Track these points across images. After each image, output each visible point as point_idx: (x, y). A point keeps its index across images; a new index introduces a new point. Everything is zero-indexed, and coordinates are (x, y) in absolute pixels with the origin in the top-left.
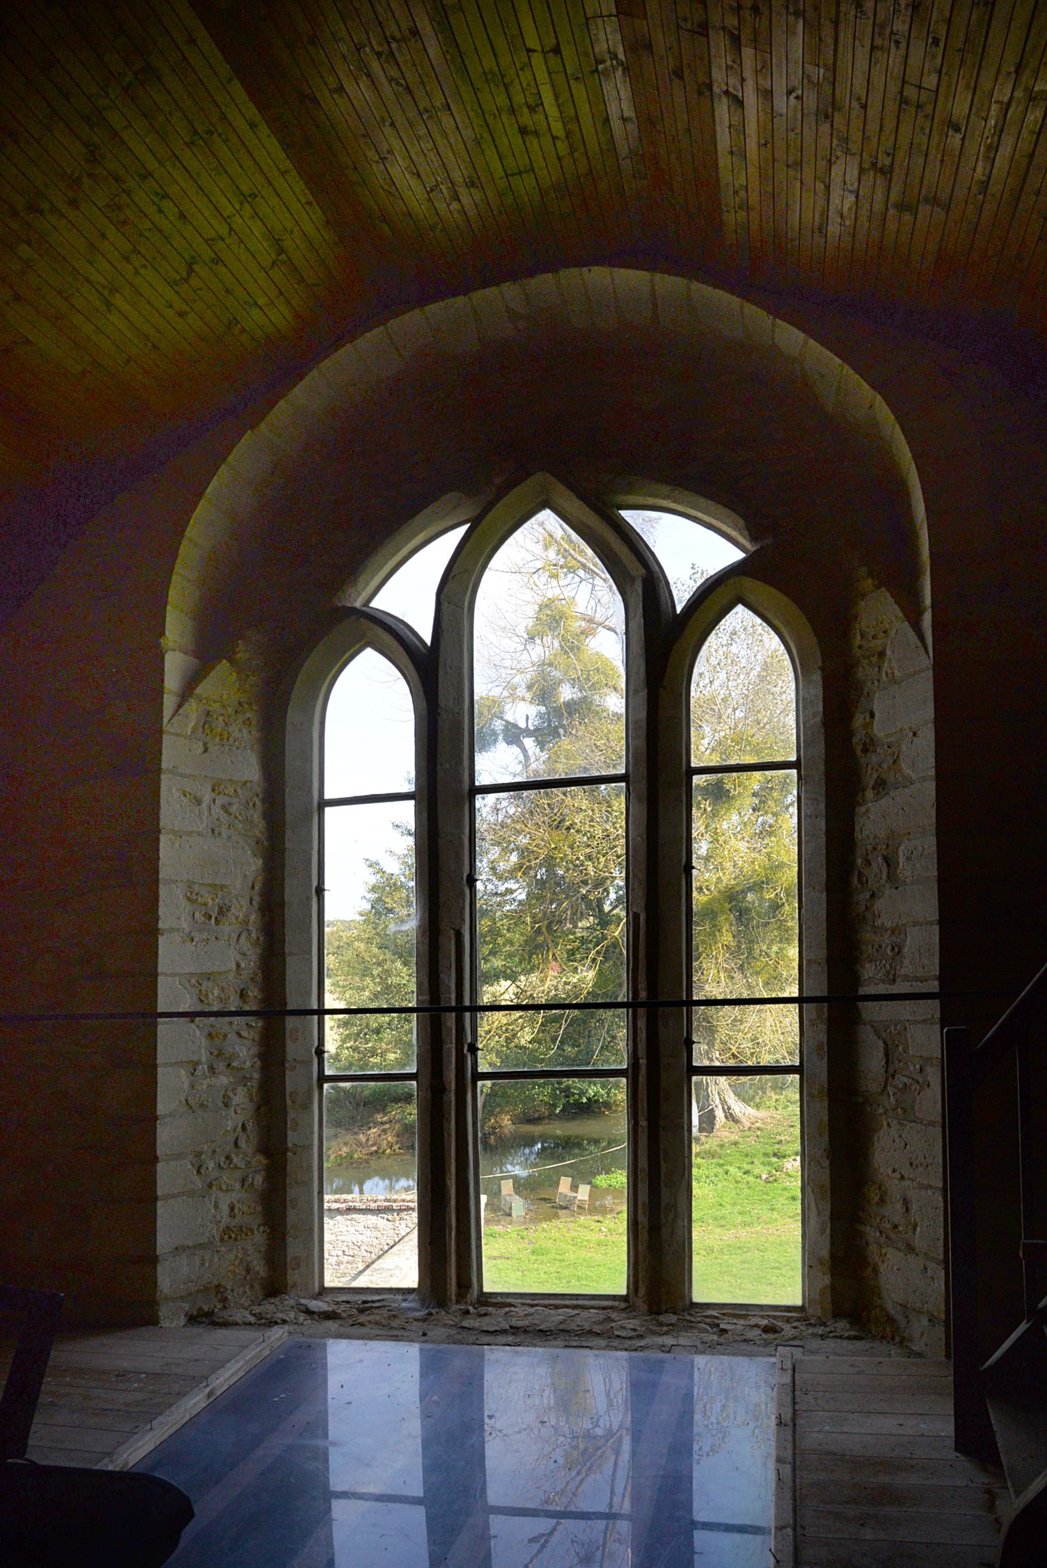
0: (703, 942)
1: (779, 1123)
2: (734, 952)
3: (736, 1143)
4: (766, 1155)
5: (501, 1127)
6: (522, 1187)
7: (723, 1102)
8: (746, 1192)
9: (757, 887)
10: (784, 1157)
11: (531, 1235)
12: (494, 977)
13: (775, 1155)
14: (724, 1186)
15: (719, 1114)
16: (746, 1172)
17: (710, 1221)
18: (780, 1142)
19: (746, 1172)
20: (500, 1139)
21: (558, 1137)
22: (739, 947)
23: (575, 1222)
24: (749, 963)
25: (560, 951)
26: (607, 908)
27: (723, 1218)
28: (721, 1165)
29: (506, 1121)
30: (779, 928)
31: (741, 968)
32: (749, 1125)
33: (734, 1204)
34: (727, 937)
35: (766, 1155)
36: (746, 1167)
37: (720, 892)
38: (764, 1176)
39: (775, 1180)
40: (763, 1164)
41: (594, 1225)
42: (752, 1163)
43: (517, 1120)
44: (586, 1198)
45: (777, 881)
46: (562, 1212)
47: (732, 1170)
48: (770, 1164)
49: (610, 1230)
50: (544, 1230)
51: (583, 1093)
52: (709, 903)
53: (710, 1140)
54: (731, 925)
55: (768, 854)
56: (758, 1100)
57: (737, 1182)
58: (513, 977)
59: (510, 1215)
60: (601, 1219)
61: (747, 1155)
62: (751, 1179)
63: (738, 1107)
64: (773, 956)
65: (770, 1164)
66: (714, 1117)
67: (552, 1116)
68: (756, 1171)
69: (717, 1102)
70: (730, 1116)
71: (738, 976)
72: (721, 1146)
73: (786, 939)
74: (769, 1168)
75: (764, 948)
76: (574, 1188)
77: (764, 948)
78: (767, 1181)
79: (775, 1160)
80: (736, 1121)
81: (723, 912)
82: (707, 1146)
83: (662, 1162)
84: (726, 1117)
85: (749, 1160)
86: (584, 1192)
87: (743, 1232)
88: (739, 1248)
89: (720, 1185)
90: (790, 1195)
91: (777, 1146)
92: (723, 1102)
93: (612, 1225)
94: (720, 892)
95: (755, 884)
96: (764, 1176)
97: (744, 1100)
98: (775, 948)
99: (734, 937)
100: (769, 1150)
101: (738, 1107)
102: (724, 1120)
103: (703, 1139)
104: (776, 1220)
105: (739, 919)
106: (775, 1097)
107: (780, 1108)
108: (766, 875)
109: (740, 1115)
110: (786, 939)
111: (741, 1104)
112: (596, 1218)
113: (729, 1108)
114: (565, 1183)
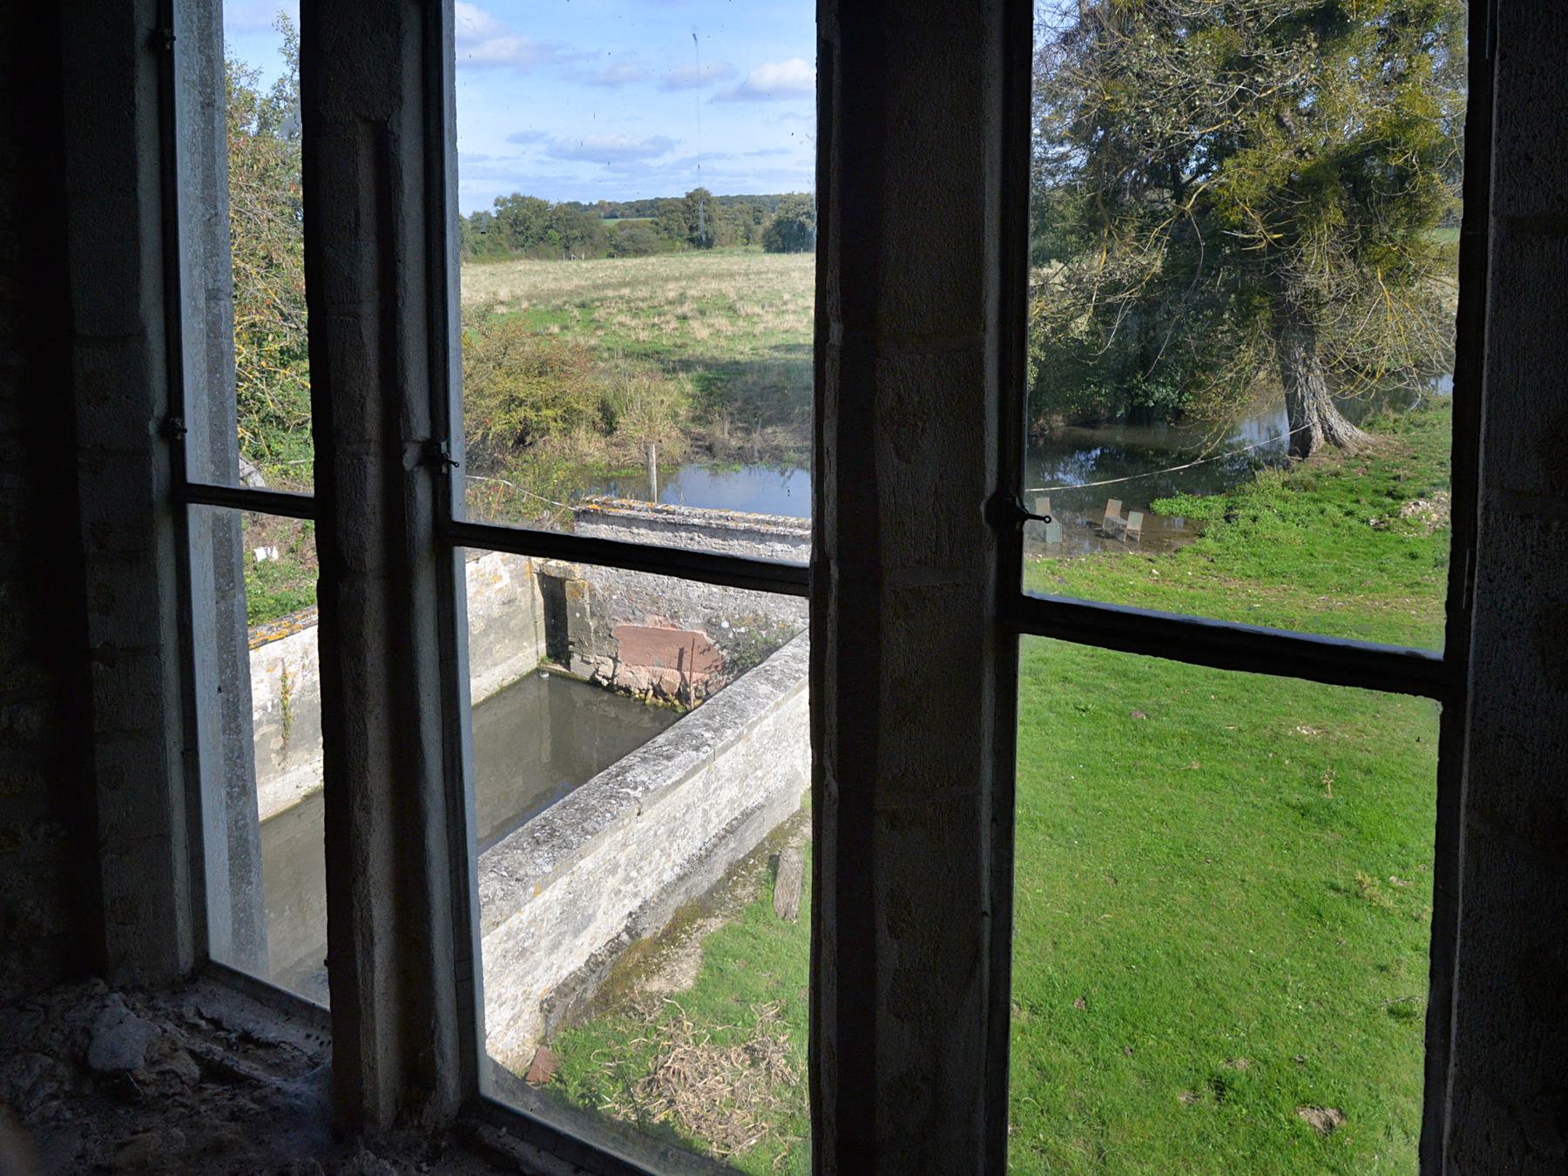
0: (1303, 220)
1: (1398, 452)
2: (1346, 234)
3: (1337, 474)
4: (1376, 491)
5: (1051, 429)
6: (1065, 502)
7: (1323, 420)
8: (1347, 540)
9: (1381, 149)
10: (1402, 498)
11: (1064, 570)
12: (1044, 258)
13: (1389, 494)
14: (1317, 530)
15: (1318, 434)
16: (1349, 513)
17: (1295, 577)
18: (1396, 478)
19: (1349, 513)
20: (1049, 441)
21: (1118, 445)
22: (1350, 228)
23: (1121, 558)
24: (1364, 249)
25: (1130, 230)
26: (1186, 176)
27: (1313, 575)
28: (1315, 501)
29: (1058, 421)
30: (1408, 205)
31: (1353, 255)
32: (1356, 451)
33: (1329, 556)
34: (1335, 215)
35: (1376, 491)
36: (1350, 506)
37: (1327, 156)
38: (1373, 521)
39: (1388, 529)
40: (1371, 504)
41: (1144, 564)
42: (1358, 501)
43: (1071, 422)
44: (1138, 528)
45: (1406, 143)
46: (1108, 542)
47: (1331, 509)
48: (1381, 505)
49: (1162, 573)
50: (1081, 565)
51: (1148, 395)
52: (1311, 170)
53: (1302, 466)
54: (1341, 198)
55: (1396, 107)
56: (1370, 419)
57: (1336, 526)
58: (1063, 256)
59: (1044, 540)
60: (1154, 557)
61: (1351, 491)
62: (1354, 522)
63: (1342, 428)
64: (1398, 240)
65: (1381, 505)
66: (1311, 438)
67: (1112, 420)
68: (1363, 514)
69: (1315, 419)
70: (1331, 437)
71: (1349, 265)
72: (1318, 476)
73: (1418, 220)
74: (1381, 511)
75: (1386, 230)
76: (1125, 512)
77: (1386, 230)
78: (1377, 529)
79: (1389, 500)
80: (1340, 445)
81: (1332, 183)
82: (1298, 475)
83: (883, 935)
84: (1326, 439)
85: (1354, 497)
86: (1135, 522)
87: (1337, 602)
88: (1330, 625)
89: (1310, 529)
90: (1407, 550)
91: (1393, 483)
92: (1323, 420)
93: (1166, 567)
94: (1327, 156)
95: (1376, 146)
96: (1373, 521)
97: (1350, 419)
98: (1401, 231)
99: (1345, 215)
100: (1382, 486)
101: (1342, 428)
102: (1323, 442)
103: (1294, 465)
104: (1386, 587)
105: (1354, 193)
106: (1393, 416)
107: (1399, 431)
108: (1393, 134)
109: (1345, 439)
110: (1418, 220)
111: (1348, 425)
112: (1147, 555)
113: (1331, 428)
114: (1113, 508)
